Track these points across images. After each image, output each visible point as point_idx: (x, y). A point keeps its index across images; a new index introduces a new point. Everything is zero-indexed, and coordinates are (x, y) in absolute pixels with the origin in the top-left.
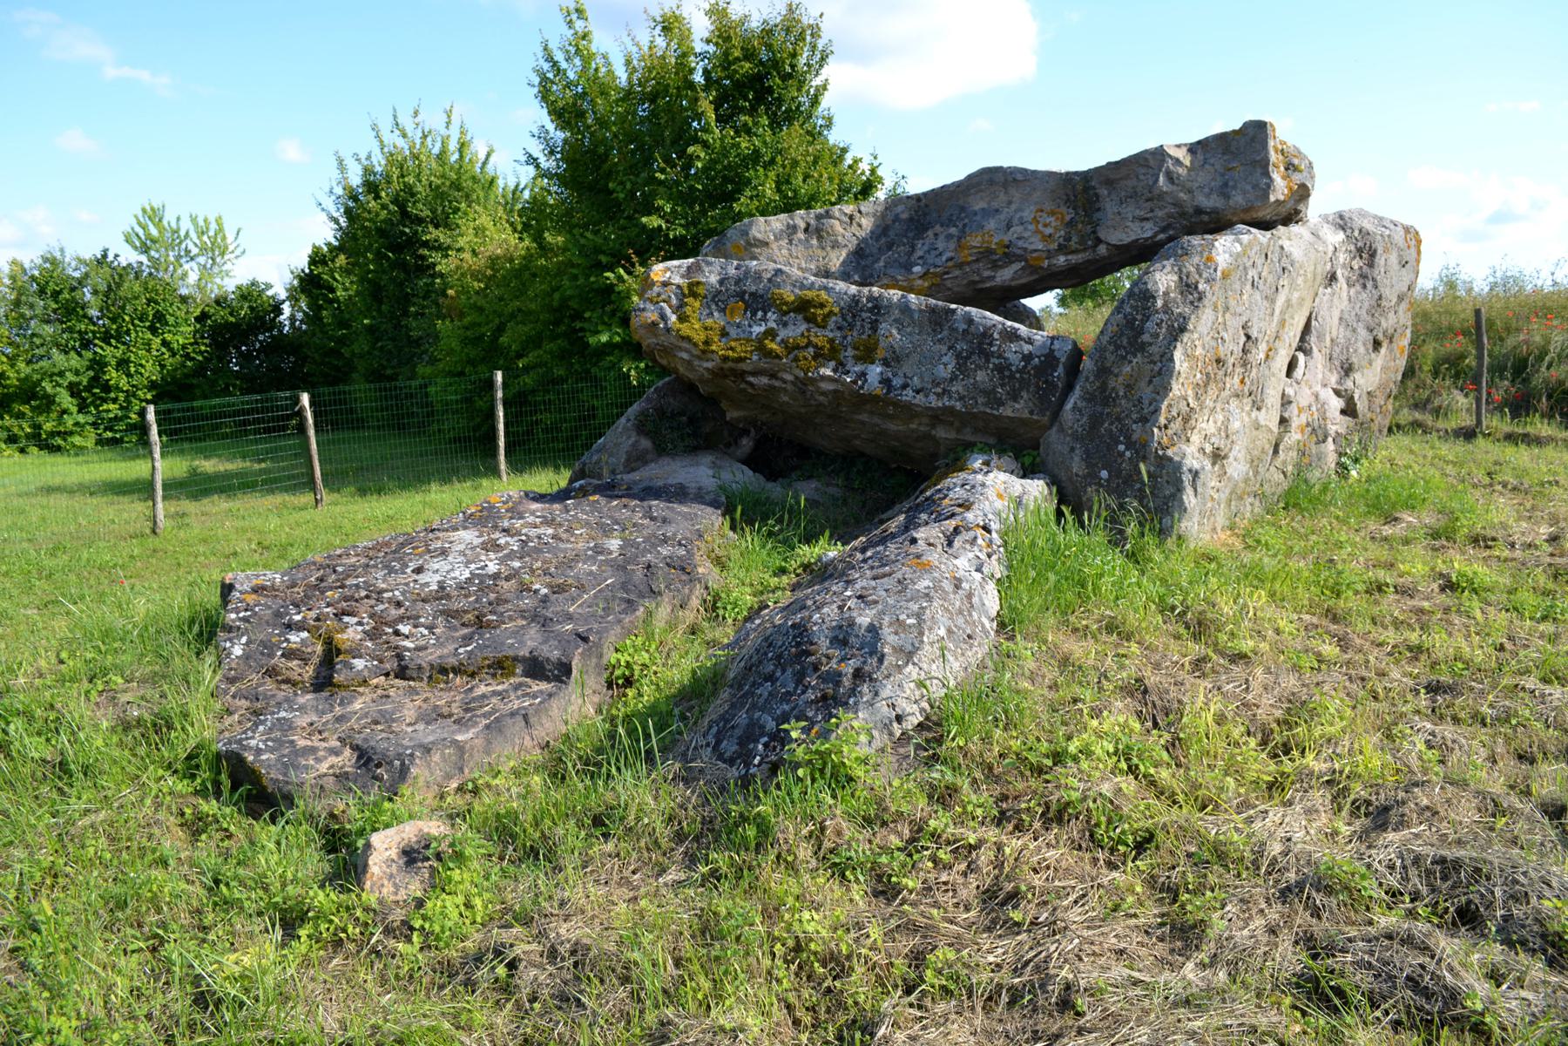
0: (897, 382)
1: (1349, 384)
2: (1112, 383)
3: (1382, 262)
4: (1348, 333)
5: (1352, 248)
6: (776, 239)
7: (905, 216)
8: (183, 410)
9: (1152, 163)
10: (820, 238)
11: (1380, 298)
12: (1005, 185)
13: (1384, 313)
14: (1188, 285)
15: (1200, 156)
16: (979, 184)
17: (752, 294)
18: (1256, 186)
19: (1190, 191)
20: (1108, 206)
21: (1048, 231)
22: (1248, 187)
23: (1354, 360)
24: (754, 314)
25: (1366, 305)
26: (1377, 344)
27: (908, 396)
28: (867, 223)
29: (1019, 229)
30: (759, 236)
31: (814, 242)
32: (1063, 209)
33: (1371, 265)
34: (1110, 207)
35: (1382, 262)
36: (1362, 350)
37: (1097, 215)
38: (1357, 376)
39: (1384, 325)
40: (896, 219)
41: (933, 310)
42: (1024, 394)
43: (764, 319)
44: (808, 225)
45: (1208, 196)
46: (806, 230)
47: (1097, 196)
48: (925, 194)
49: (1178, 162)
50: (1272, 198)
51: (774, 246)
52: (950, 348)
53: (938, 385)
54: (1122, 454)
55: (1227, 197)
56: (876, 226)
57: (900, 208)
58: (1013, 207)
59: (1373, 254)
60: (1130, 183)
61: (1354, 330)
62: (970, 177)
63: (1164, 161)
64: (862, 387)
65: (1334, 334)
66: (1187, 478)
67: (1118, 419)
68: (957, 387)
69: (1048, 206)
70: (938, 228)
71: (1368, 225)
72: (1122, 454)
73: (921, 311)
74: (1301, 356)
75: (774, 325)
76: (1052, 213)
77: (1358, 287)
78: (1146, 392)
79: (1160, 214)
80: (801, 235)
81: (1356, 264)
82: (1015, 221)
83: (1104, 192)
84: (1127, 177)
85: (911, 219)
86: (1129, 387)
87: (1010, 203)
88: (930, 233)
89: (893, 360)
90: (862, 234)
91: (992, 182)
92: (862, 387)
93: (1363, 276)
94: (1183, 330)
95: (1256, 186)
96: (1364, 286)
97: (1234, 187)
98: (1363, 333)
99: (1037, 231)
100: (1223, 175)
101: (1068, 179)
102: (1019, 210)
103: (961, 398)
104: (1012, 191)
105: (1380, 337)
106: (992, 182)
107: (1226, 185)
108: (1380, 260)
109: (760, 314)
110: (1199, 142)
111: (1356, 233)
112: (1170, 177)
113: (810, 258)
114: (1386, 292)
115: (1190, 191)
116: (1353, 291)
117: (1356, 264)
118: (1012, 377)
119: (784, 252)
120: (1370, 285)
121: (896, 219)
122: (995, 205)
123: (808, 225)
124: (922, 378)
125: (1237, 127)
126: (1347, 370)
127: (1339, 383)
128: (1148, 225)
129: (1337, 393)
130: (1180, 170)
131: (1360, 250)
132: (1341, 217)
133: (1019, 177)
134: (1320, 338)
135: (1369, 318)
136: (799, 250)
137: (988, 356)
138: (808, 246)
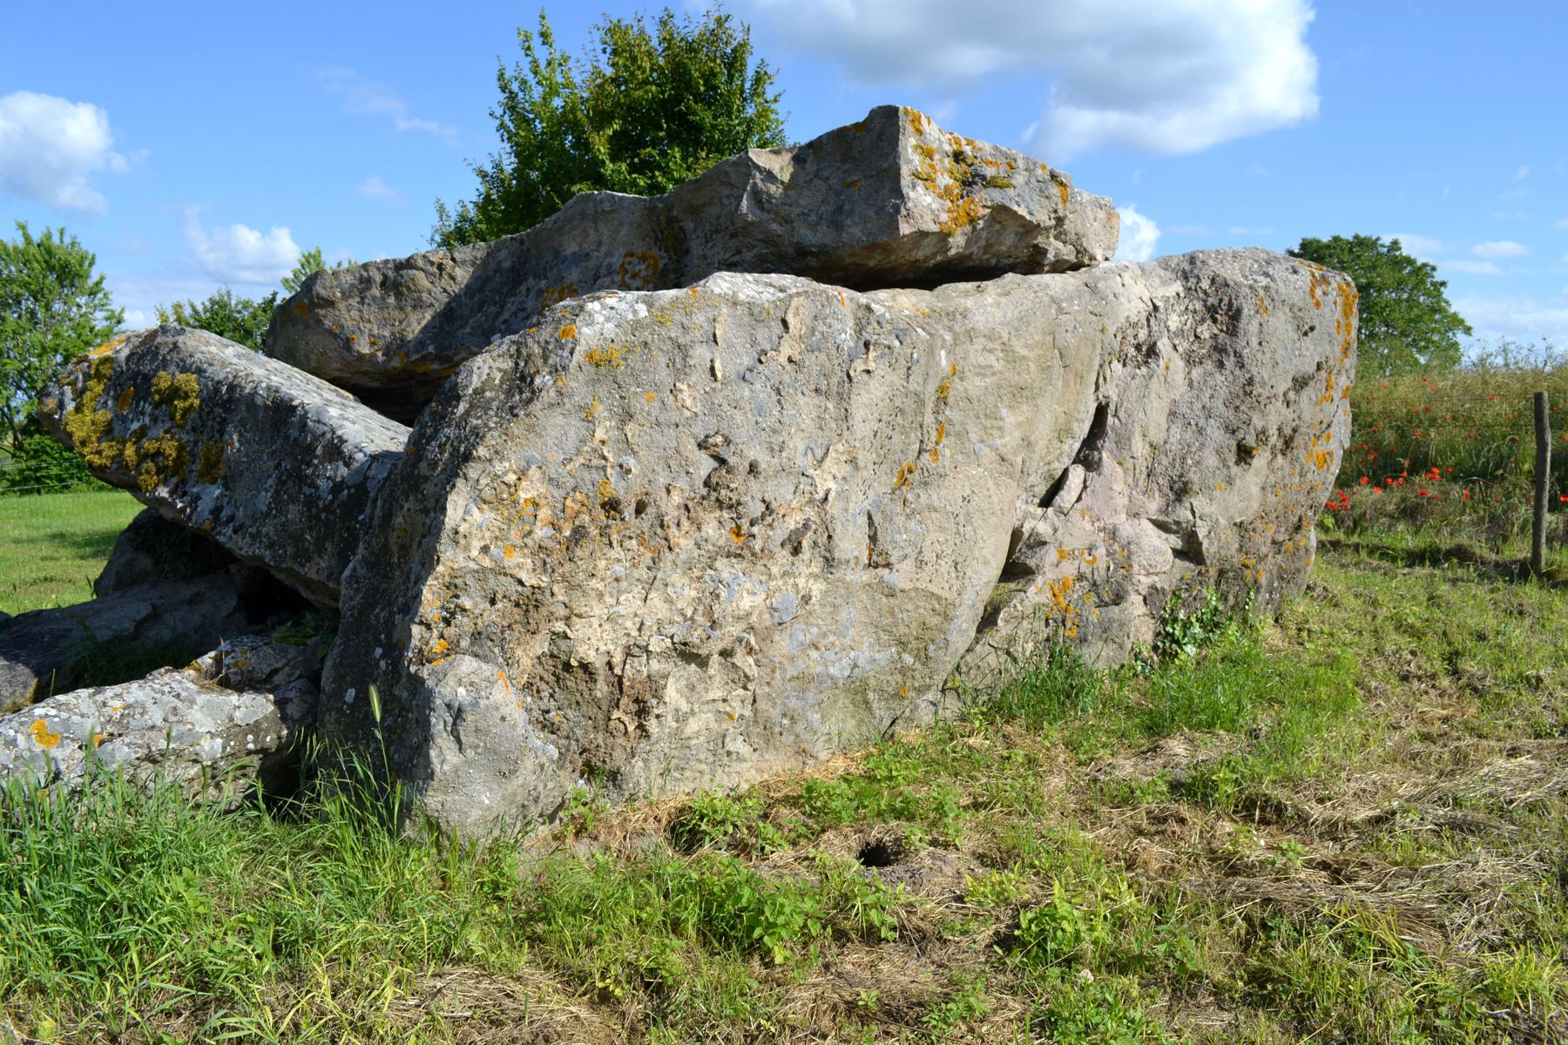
1: (1183, 514)
3: (1253, 328)
4: (1188, 436)
5: (1199, 306)
6: (345, 296)
7: (507, 264)
9: (734, 178)
10: (399, 295)
11: (1250, 382)
13: (1260, 405)
14: (523, 378)
15: (810, 166)
18: (880, 210)
19: (787, 221)
22: (871, 212)
23: (1194, 477)
25: (1223, 393)
26: (1244, 454)
28: (463, 275)
30: (323, 292)
31: (392, 300)
32: (655, 252)
33: (1233, 332)
35: (1253, 328)
36: (1211, 460)
38: (1199, 502)
39: (1258, 422)
40: (498, 269)
42: (328, 545)
44: (385, 276)
45: (814, 227)
46: (383, 284)
49: (770, 176)
50: (905, 229)
51: (342, 306)
55: (838, 226)
56: (474, 278)
58: (604, 249)
59: (1235, 316)
61: (1200, 431)
63: (749, 175)
64: (189, 518)
65: (1157, 436)
66: (439, 722)
68: (268, 529)
69: (639, 249)
71: (1232, 272)
73: (266, 407)
74: (1077, 474)
76: (643, 258)
77: (1209, 365)
80: (376, 291)
81: (1206, 331)
83: (689, 225)
85: (512, 269)
88: (523, 288)
90: (455, 289)
92: (189, 518)
93: (1219, 349)
94: (467, 457)
95: (880, 210)
96: (1221, 365)
97: (850, 213)
98: (1215, 434)
100: (838, 194)
103: (271, 546)
105: (1250, 441)
107: (840, 210)
108: (1249, 326)
110: (811, 145)
111: (1205, 284)
112: (756, 195)
113: (384, 323)
114: (1262, 373)
115: (787, 221)
116: (1196, 373)
117: (1206, 331)
119: (354, 313)
120: (1230, 362)
121: (498, 269)
123: (385, 276)
125: (861, 117)
126: (1180, 491)
127: (1165, 512)
129: (1161, 526)
130: (773, 189)
131: (1212, 311)
132: (1192, 260)
134: (1123, 442)
135: (1230, 413)
136: (371, 312)
138: (383, 306)
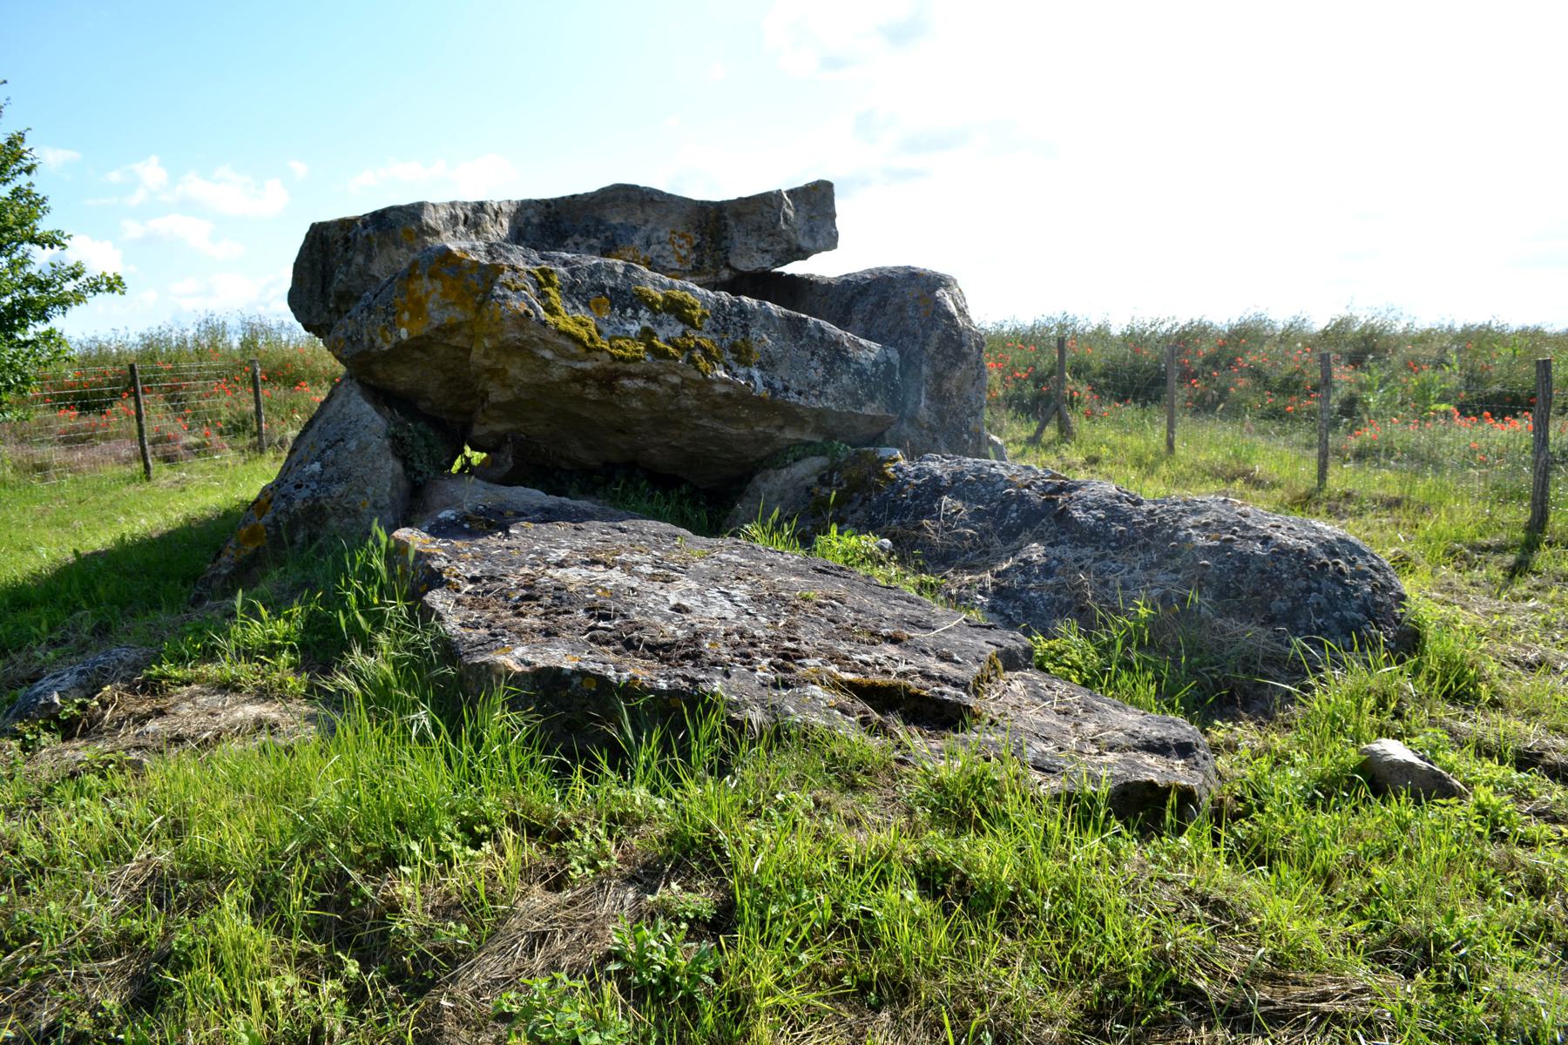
0: (778, 385)
2: (946, 385)
7: (535, 220)
8: (944, 680)
12: (642, 204)
16: (614, 199)
17: (611, 289)
20: (736, 235)
21: (683, 253)
24: (623, 311)
27: (793, 398)
29: (658, 248)
30: (431, 223)
32: (692, 234)
34: (737, 237)
37: (724, 243)
40: (528, 223)
41: (788, 318)
43: (636, 317)
47: (726, 225)
48: (555, 201)
52: (813, 354)
53: (813, 387)
54: (966, 442)
57: (530, 212)
58: (649, 226)
60: (757, 218)
62: (603, 191)
67: (955, 414)
68: (830, 390)
70: (577, 238)
72: (966, 442)
75: (648, 324)
76: (682, 236)
78: (971, 391)
79: (778, 248)
82: (654, 240)
83: (732, 223)
84: (753, 213)
85: (541, 225)
86: (959, 389)
87: (646, 221)
89: (768, 364)
91: (628, 199)
99: (675, 252)
101: (703, 206)
102: (654, 229)
104: (649, 210)
106: (628, 199)
109: (629, 311)
118: (868, 380)
122: (632, 221)
123: (466, 217)
124: (798, 381)
128: (768, 257)
133: (656, 198)
137: (848, 361)
